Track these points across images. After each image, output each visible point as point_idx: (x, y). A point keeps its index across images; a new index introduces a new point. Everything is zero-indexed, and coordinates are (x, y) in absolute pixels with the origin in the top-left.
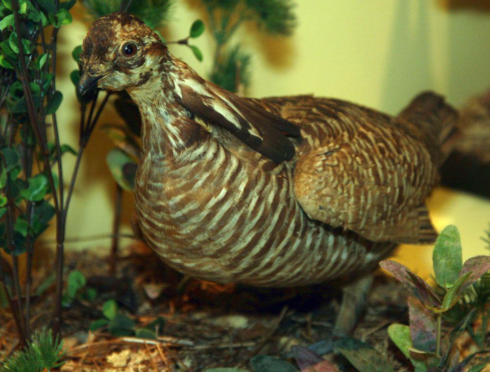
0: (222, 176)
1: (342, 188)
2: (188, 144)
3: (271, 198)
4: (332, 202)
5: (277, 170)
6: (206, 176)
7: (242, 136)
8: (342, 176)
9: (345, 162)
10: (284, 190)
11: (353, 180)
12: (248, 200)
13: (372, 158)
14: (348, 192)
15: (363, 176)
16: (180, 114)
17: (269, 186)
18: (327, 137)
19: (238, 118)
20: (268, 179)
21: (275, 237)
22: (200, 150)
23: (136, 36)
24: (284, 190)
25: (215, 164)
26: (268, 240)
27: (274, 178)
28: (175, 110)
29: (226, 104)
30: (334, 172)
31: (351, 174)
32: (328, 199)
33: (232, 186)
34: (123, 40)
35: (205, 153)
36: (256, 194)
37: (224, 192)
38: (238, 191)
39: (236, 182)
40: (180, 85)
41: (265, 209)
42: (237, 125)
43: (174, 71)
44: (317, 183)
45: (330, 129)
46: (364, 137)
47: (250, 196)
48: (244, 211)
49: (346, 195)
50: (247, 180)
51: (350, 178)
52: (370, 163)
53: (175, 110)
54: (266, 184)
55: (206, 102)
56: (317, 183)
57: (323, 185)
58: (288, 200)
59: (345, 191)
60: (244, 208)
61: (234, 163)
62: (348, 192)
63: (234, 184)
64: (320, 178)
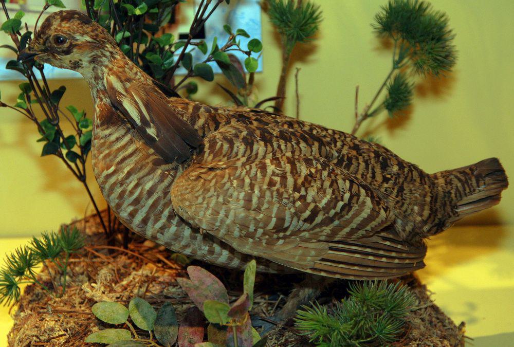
0: (115, 157)
1: (204, 199)
2: (102, 125)
3: (148, 186)
4: (190, 206)
5: (164, 167)
6: (107, 152)
7: (139, 131)
8: (208, 190)
9: (219, 180)
10: (166, 183)
11: (218, 196)
12: (128, 181)
13: (252, 186)
14: (208, 204)
15: (231, 196)
16: (104, 100)
17: (151, 176)
18: (221, 157)
19: (141, 114)
20: (152, 171)
21: (150, 218)
22: (107, 132)
23: (66, 31)
24: (166, 183)
25: (114, 145)
26: (144, 217)
27: (159, 172)
28: (102, 96)
29: (136, 103)
30: (204, 184)
31: (218, 191)
32: (187, 203)
33: (119, 166)
34: (55, 32)
35: (110, 135)
36: (136, 179)
37: (113, 169)
38: (123, 172)
39: (123, 165)
40: (107, 78)
41: (141, 193)
42: (138, 122)
43: (106, 67)
44: (184, 187)
45: (229, 152)
46: (263, 168)
47: (131, 178)
48: (125, 188)
49: (205, 205)
50: (132, 166)
51: (215, 194)
52: (247, 188)
53: (102, 96)
54: (149, 174)
55: (119, 97)
56: (184, 187)
57: (188, 191)
58: (166, 193)
59: (205, 202)
60: (124, 186)
61: (131, 149)
62: (208, 204)
63: (121, 165)
64: (189, 185)
